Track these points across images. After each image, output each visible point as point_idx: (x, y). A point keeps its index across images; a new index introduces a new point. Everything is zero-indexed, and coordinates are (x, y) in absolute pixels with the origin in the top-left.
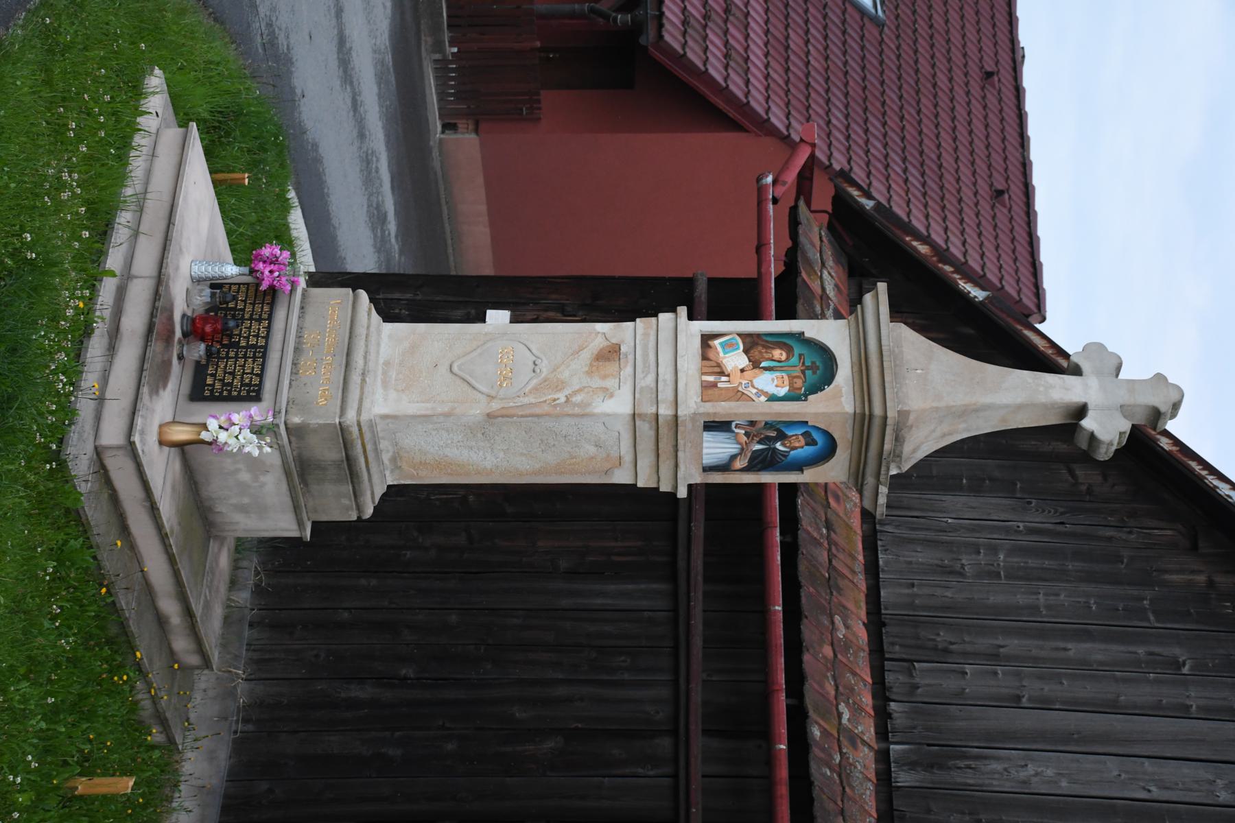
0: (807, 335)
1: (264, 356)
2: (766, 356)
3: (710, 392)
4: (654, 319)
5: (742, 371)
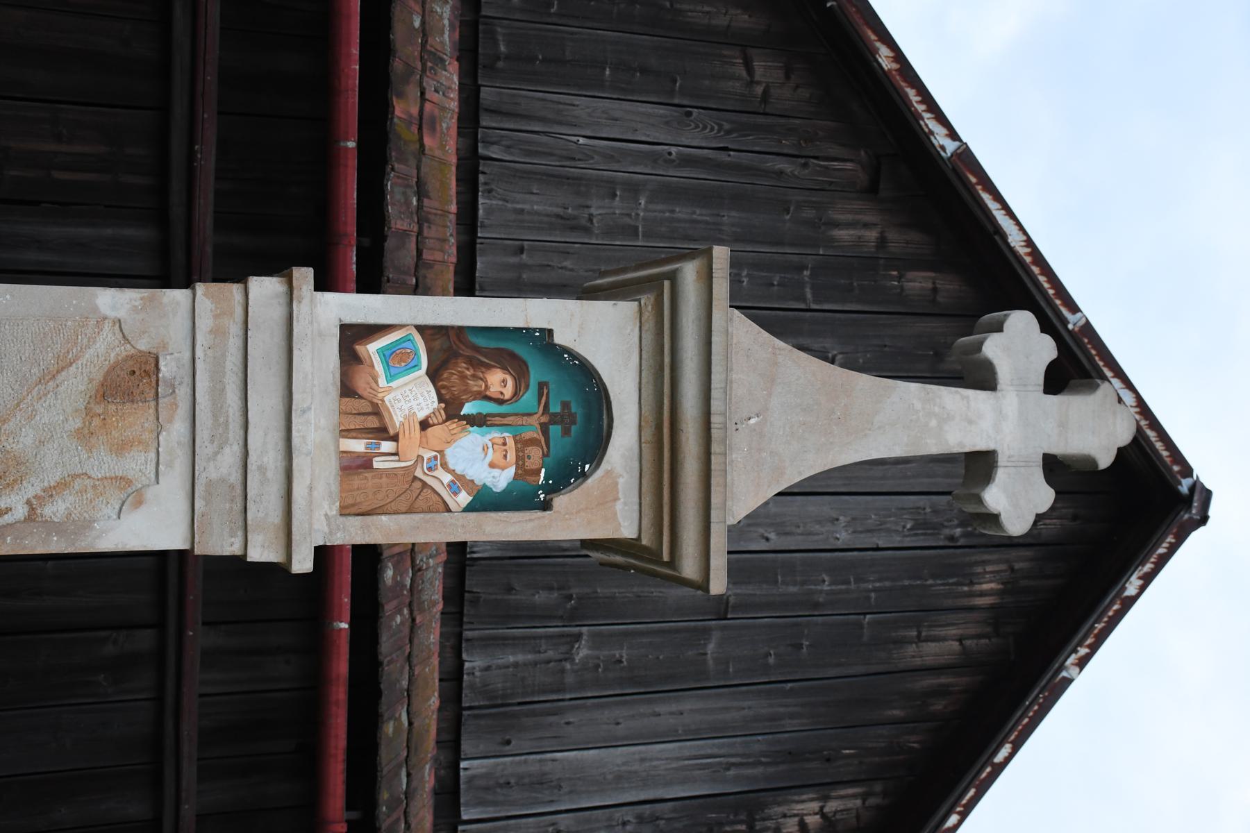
0: (559, 339)
2: (475, 386)
3: (356, 481)
4: (235, 289)
5: (425, 425)
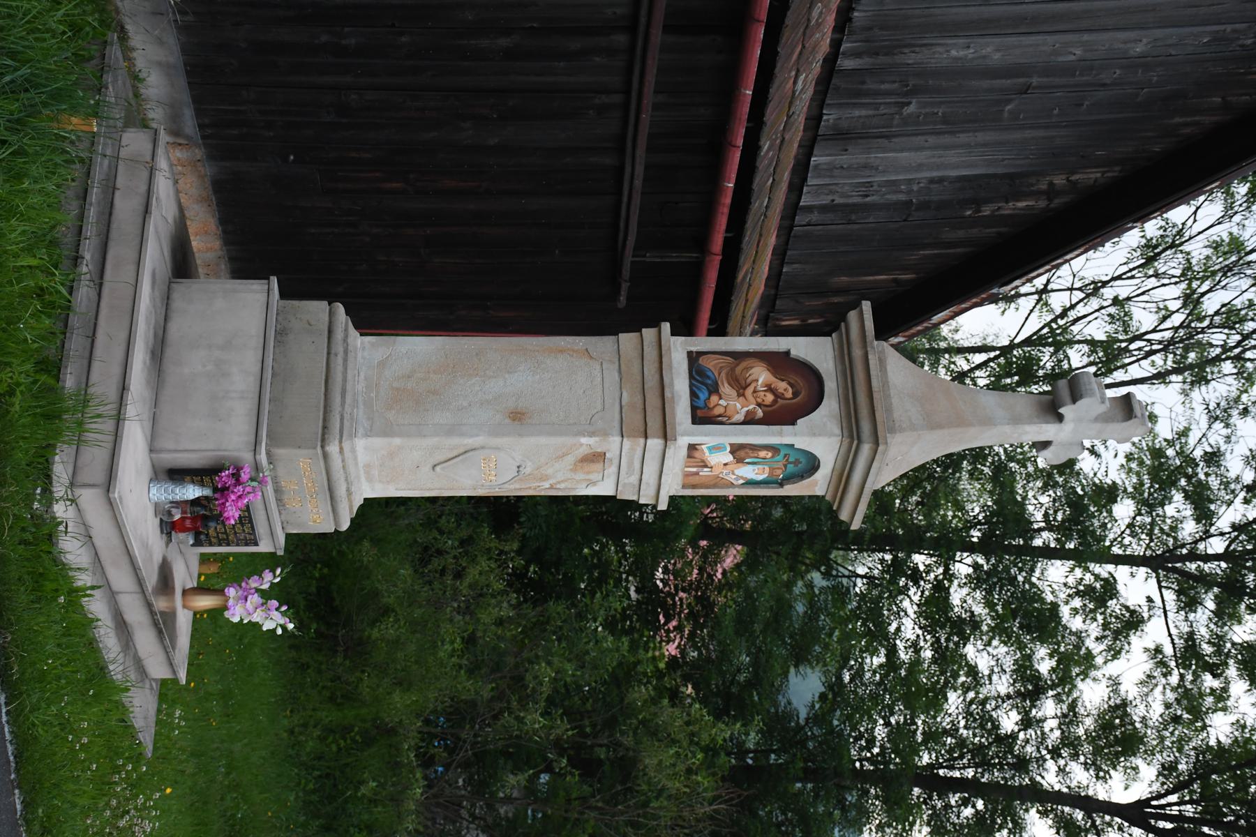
1: (251, 522)
